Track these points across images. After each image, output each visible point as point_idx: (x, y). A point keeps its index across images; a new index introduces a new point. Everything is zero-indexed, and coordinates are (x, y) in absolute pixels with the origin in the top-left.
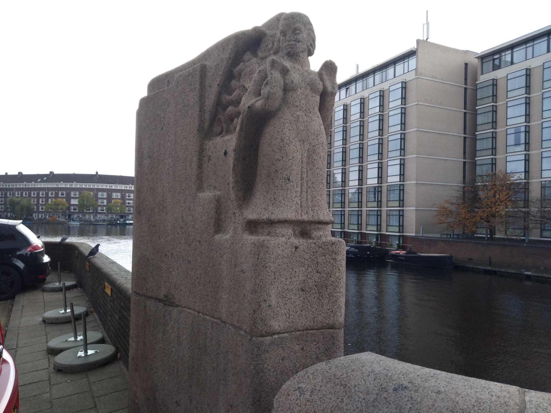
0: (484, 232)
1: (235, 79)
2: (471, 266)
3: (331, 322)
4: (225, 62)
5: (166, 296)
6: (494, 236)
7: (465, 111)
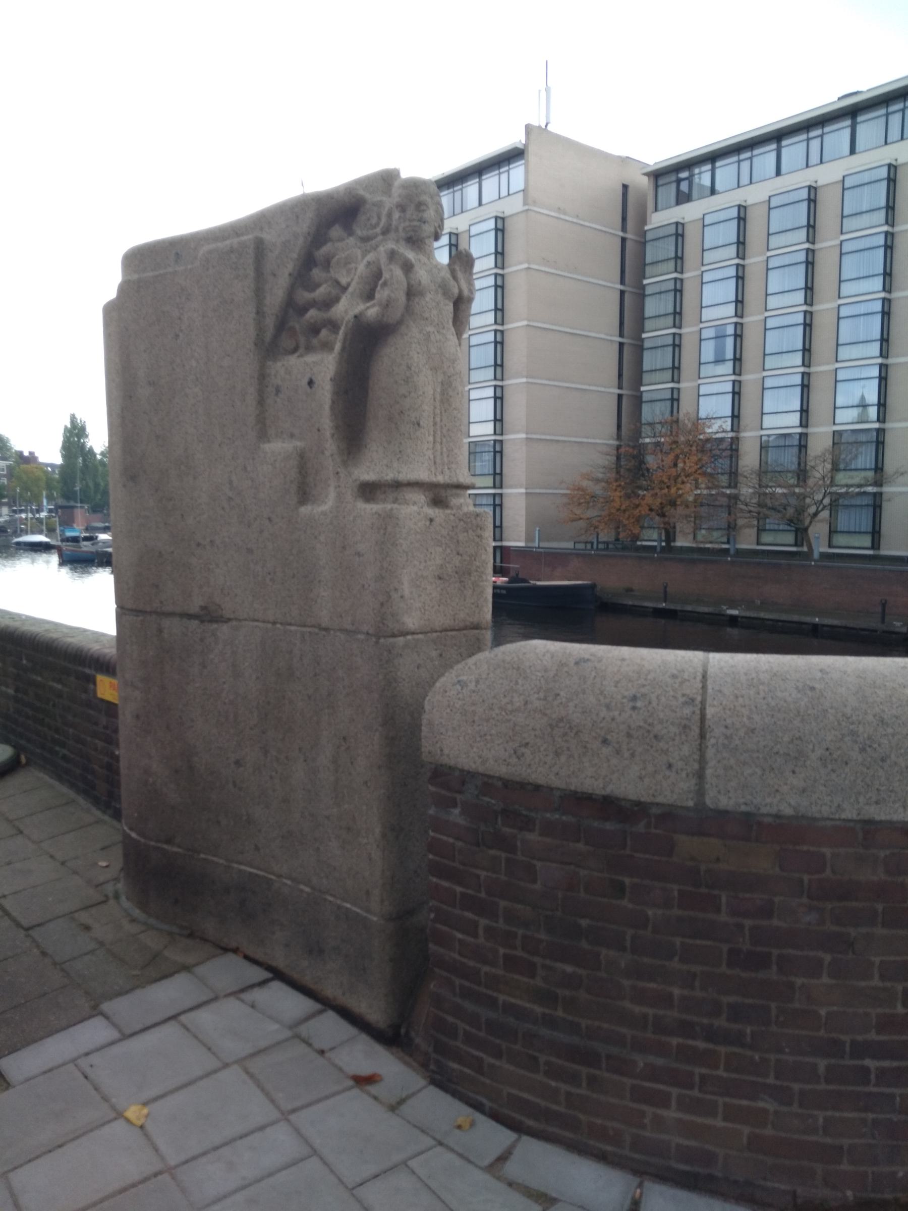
0: (655, 536)
1: (316, 266)
2: (630, 603)
3: (475, 619)
4: (301, 241)
5: (204, 608)
6: (672, 544)
7: (622, 288)
